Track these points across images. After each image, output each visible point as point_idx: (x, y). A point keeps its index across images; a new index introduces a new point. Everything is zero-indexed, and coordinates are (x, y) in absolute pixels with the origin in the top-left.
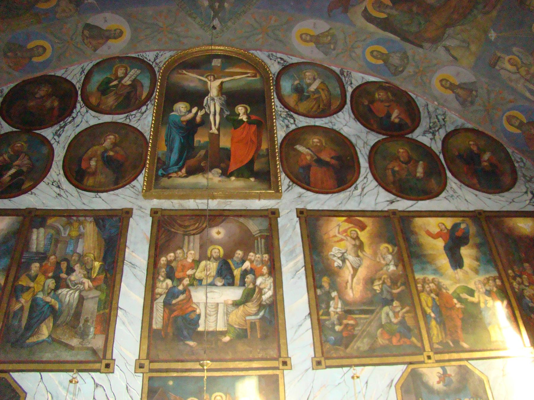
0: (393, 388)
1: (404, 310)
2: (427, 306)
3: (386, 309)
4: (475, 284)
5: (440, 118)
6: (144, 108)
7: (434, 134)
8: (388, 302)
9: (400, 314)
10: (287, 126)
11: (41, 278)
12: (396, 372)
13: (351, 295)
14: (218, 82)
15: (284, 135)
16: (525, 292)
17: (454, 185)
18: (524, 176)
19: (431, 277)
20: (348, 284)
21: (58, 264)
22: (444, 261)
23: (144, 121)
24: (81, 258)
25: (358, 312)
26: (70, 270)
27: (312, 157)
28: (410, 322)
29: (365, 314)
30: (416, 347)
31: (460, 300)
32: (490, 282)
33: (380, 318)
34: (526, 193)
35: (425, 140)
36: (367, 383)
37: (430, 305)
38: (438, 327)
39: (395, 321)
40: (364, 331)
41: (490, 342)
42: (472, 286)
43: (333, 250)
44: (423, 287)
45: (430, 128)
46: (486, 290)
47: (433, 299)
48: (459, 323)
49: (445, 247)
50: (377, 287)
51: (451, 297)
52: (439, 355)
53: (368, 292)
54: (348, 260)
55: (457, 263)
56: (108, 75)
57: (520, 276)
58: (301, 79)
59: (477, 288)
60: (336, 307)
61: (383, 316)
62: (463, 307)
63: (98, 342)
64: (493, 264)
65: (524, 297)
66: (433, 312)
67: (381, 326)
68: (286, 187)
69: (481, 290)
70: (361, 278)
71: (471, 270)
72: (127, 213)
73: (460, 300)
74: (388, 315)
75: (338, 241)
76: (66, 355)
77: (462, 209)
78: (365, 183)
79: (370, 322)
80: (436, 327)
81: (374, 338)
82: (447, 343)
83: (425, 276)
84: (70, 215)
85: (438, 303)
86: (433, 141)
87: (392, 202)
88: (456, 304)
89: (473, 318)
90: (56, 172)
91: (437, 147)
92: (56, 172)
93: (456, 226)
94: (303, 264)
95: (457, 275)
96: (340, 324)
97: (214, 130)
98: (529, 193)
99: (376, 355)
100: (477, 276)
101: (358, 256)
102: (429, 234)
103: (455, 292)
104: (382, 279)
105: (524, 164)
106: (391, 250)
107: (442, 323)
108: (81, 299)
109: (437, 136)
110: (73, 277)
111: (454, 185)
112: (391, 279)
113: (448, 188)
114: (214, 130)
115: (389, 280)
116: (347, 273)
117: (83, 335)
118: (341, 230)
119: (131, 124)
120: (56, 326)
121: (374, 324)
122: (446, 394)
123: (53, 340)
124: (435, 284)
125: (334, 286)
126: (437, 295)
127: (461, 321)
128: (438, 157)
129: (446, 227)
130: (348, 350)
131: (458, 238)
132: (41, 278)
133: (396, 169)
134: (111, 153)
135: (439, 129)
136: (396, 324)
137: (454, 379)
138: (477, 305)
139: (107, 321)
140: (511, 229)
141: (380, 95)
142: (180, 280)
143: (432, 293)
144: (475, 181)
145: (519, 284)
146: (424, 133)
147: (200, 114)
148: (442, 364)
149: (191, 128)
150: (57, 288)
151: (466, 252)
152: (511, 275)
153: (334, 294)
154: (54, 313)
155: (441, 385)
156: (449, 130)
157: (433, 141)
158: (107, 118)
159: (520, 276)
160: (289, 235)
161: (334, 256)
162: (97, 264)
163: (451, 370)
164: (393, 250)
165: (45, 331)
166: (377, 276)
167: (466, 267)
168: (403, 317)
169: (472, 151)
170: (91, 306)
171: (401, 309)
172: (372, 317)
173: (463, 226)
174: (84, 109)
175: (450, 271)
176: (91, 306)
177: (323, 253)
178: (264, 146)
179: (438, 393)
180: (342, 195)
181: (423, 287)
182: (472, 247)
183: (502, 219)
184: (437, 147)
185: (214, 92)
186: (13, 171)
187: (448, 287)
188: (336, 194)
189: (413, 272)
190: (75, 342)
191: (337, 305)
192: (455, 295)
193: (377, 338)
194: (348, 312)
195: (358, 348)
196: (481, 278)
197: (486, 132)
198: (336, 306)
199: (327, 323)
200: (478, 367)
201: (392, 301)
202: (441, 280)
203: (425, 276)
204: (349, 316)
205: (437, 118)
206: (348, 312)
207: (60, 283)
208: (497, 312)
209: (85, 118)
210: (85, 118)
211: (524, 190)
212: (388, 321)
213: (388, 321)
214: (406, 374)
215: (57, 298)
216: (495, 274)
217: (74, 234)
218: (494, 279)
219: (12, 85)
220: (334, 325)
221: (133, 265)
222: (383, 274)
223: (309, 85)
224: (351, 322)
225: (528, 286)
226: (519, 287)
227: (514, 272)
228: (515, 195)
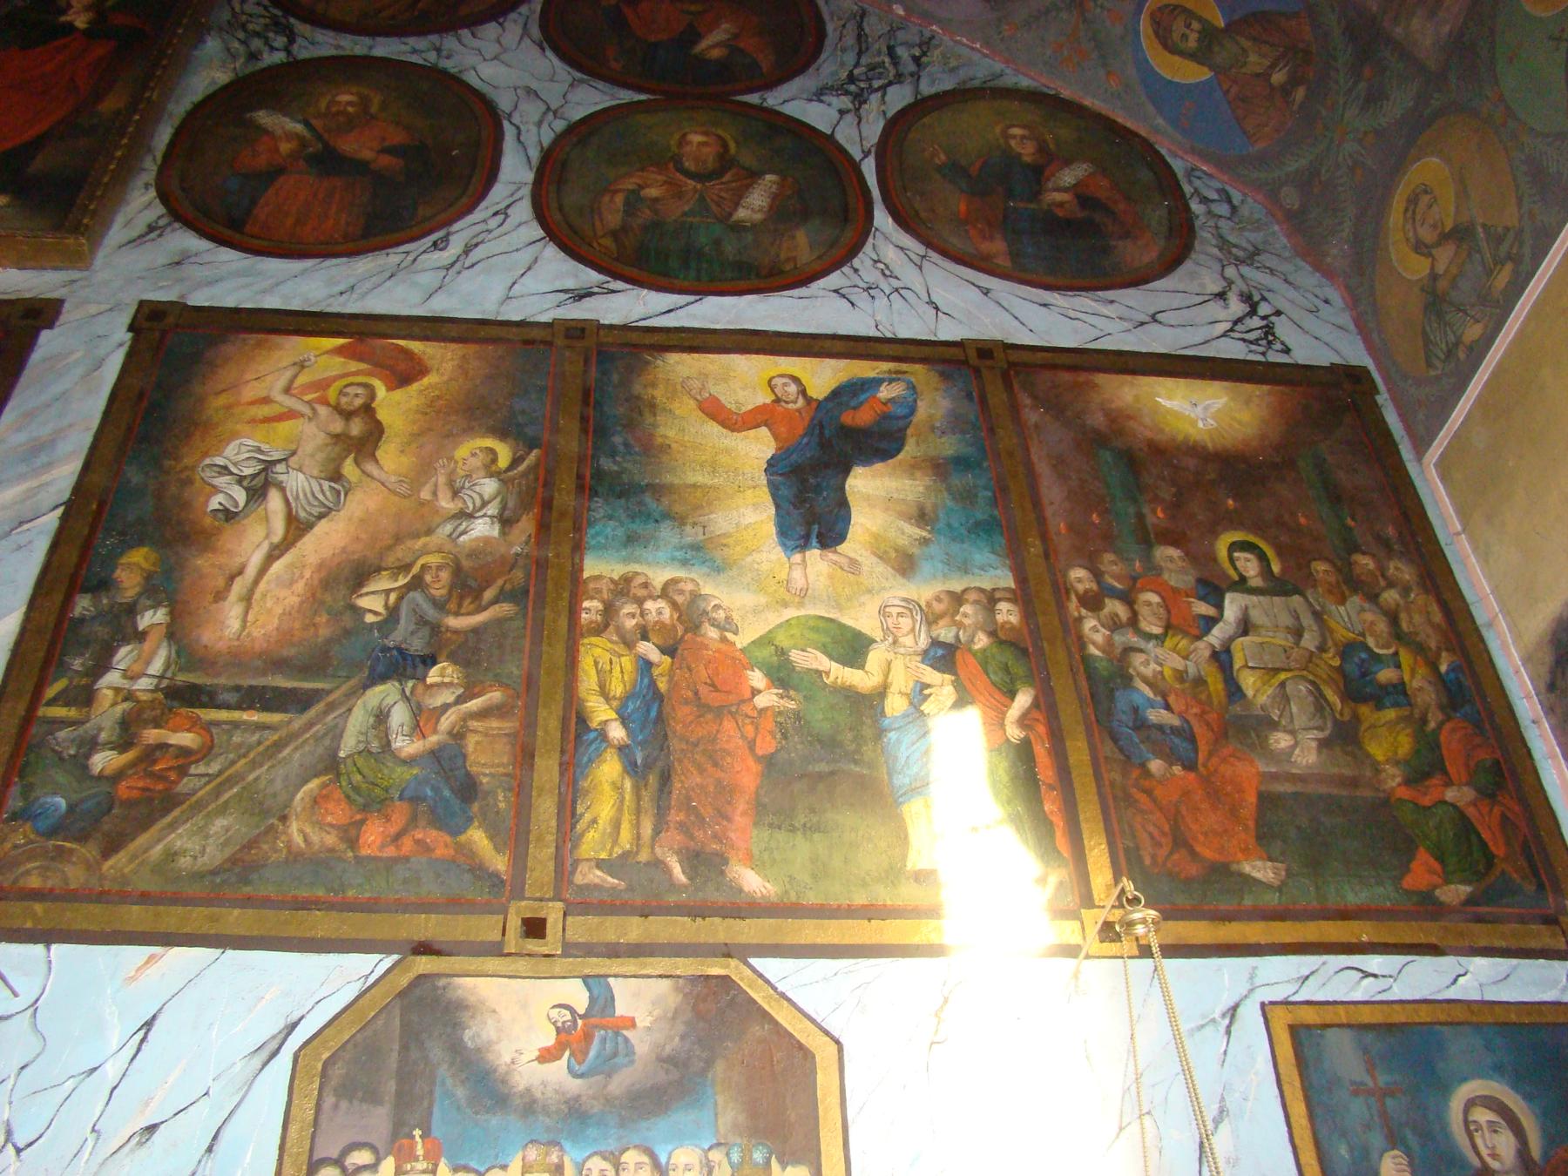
0: (284, 1060)
1: (474, 704)
2: (604, 692)
3: (385, 693)
4: (883, 611)
8: (403, 666)
9: (446, 722)
10: (253, 56)
13: (234, 624)
15: (223, 77)
16: (1137, 660)
17: (890, 255)
18: (1224, 244)
19: (660, 576)
20: (238, 580)
22: (751, 516)
25: (232, 698)
27: (303, 143)
29: (266, 708)
30: (479, 871)
31: (782, 675)
32: (967, 608)
33: (337, 734)
34: (1221, 296)
36: (149, 1025)
37: (617, 689)
38: (628, 784)
39: (405, 745)
40: (230, 782)
41: (894, 873)
42: (863, 620)
43: (231, 450)
44: (609, 610)
45: (851, 78)
46: (935, 643)
47: (646, 665)
48: (748, 776)
49: (772, 465)
50: (372, 603)
51: (740, 662)
52: (593, 920)
53: (322, 619)
54: (283, 490)
55: (811, 513)
57: (1128, 599)
59: (886, 631)
61: (358, 720)
62: (792, 705)
64: (1000, 541)
65: (1127, 680)
66: (624, 720)
67: (332, 765)
68: (140, 227)
69: (908, 641)
70: (313, 559)
71: (882, 557)
73: (782, 675)
74: (381, 717)
75: (268, 420)
77: (904, 333)
78: (489, 231)
79: (278, 746)
80: (618, 788)
82: (658, 864)
83: (637, 568)
85: (662, 685)
86: (850, 118)
87: (581, 295)
88: (755, 692)
89: (835, 757)
93: (845, 394)
94: (66, 496)
95: (797, 574)
96: (122, 746)
98: (1233, 298)
100: (902, 581)
101: (336, 476)
102: (715, 411)
103: (765, 640)
104: (416, 570)
105: (1234, 209)
106: (504, 460)
112: (458, 571)
113: (862, 261)
115: (445, 575)
116: (251, 543)
118: (302, 379)
121: (295, 757)
122: (574, 1116)
124: (674, 605)
126: (669, 651)
127: (756, 768)
128: (856, 167)
129: (803, 392)
130: (119, 862)
131: (847, 432)
135: (890, 84)
136: (410, 762)
137: (642, 1042)
138: (867, 705)
140: (1118, 420)
143: (645, 638)
145: (1114, 625)
148: (596, 965)
151: (875, 494)
152: (1081, 588)
153: (152, 618)
155: (557, 1071)
156: (926, 89)
157: (850, 118)
159: (1128, 599)
160: (57, 389)
161: (225, 470)
164: (515, 462)
166: (400, 554)
167: (855, 544)
168: (458, 735)
169: (1011, 158)
171: (460, 700)
172: (299, 722)
175: (769, 554)
177: (177, 459)
178: (109, 105)
179: (530, 1107)
180: (364, 265)
181: (609, 610)
182: (913, 467)
183: (1082, 377)
187: (736, 616)
188: (344, 260)
189: (578, 548)
191: (148, 663)
192: (766, 653)
193: (284, 819)
195: (171, 855)
197: (1088, 102)
198: (137, 668)
199: (62, 734)
201: (430, 660)
202: (707, 589)
203: (637, 568)
204: (184, 711)
205: (891, 51)
206: (182, 696)
208: (955, 760)
211: (1216, 288)
212: (375, 746)
213: (375, 746)
214: (382, 997)
216: (1004, 579)
218: (990, 600)
220: (92, 745)
222: (425, 551)
224: (186, 739)
225: (1160, 639)
226: (1109, 642)
227: (1097, 575)
228: (1162, 301)
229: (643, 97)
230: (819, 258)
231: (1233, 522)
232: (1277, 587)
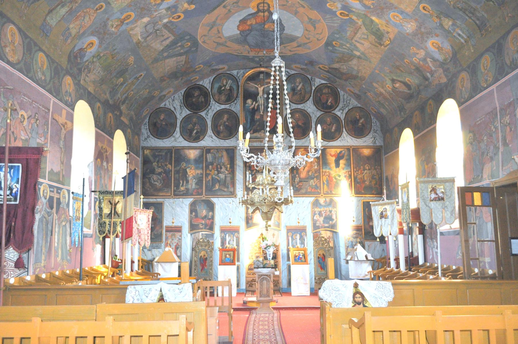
3: (312, 181)
5: (348, 102)
6: (236, 101)
7: (343, 110)
8: (313, 178)
11: (213, 171)
12: (312, 199)
14: (262, 88)
17: (344, 135)
19: (328, 170)
21: (217, 166)
22: (333, 165)
23: (237, 107)
24: (223, 164)
26: (221, 168)
28: (318, 185)
31: (336, 178)
35: (339, 113)
42: (340, 174)
55: (337, 165)
56: (220, 84)
58: (295, 83)
60: (297, 180)
63: (232, 190)
67: (310, 186)
72: (90, 229)
73: (336, 178)
76: (224, 193)
81: (307, 189)
84: (218, 149)
90: (210, 132)
91: (342, 117)
92: (210, 132)
93: (341, 152)
97: (262, 113)
99: (307, 194)
102: (331, 155)
107: (328, 185)
108: (226, 177)
109: (344, 112)
110: (222, 170)
111: (344, 135)
114: (262, 113)
117: (228, 188)
119: (232, 109)
120: (220, 185)
123: (219, 189)
125: (297, 173)
132: (213, 171)
133: (325, 128)
134: (227, 123)
139: (233, 184)
141: (325, 91)
142: (253, 170)
144: (353, 133)
146: (339, 110)
147: (256, 105)
149: (254, 111)
150: (218, 174)
151: (342, 162)
154: (219, 181)
156: (350, 108)
158: (223, 107)
162: (228, 166)
163: (328, 200)
165: (217, 187)
169: (356, 118)
170: (228, 179)
173: (343, 152)
174: (214, 102)
175: (335, 168)
176: (228, 179)
180: (304, 140)
184: (342, 117)
185: (261, 93)
186: (195, 131)
190: (226, 190)
194: (300, 181)
196: (344, 171)
200: (335, 199)
206: (300, 181)
207: (219, 172)
209: (215, 107)
210: (215, 107)
215: (218, 176)
217: (220, 155)
219: (185, 90)
221: (239, 166)
223: (298, 86)
229: (385, 187)
230: (507, 180)
231: (367, 163)
232: (369, 170)
